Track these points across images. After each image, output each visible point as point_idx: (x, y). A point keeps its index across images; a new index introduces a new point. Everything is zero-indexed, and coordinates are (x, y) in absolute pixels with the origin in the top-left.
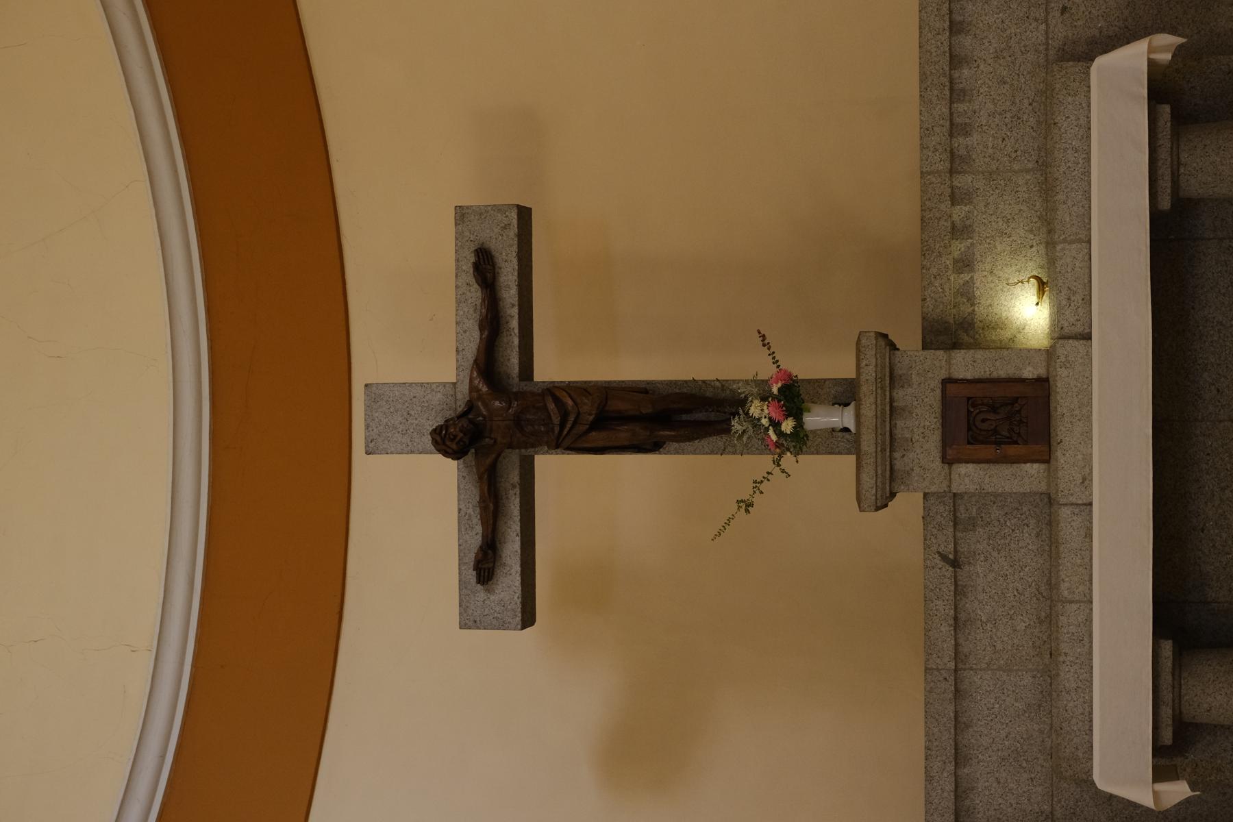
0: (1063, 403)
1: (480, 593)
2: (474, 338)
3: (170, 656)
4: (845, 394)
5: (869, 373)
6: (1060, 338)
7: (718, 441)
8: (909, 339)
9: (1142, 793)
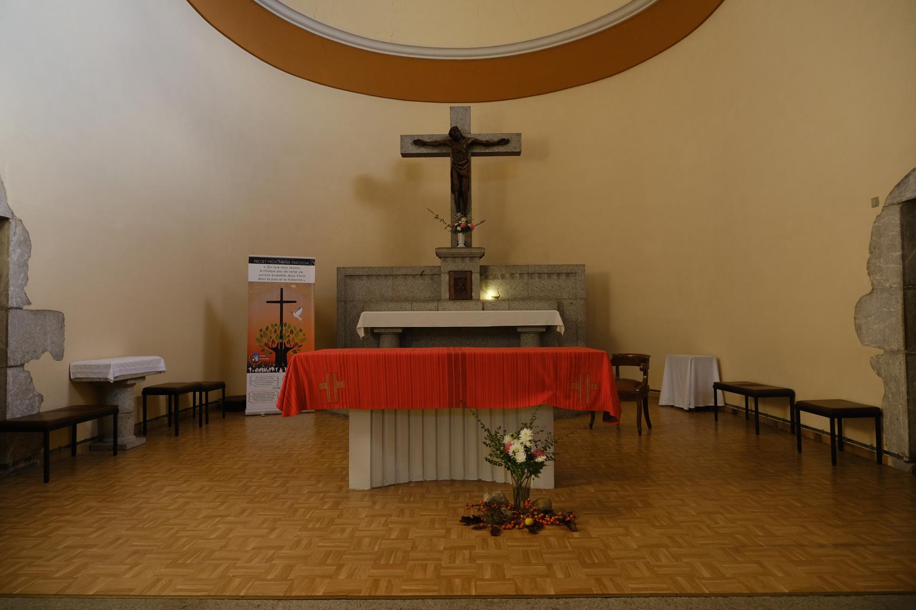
0: (465, 303)
2: (484, 139)
4: (468, 244)
5: (474, 251)
7: (454, 209)
8: (483, 262)
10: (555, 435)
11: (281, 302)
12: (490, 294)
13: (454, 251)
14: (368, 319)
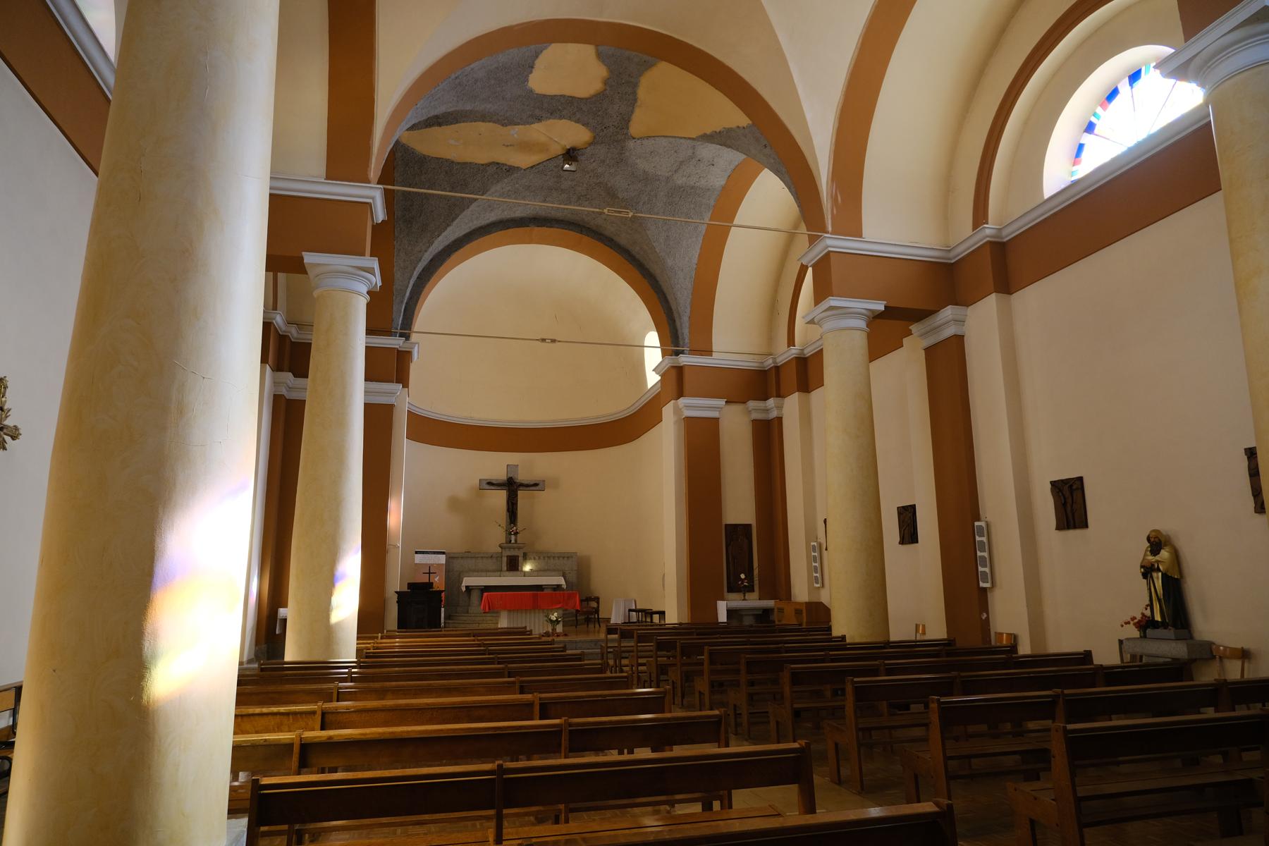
0: (515, 573)
1: (485, 482)
2: (526, 482)
3: (417, 409)
6: (540, 571)
7: (509, 521)
9: (464, 584)
11: (429, 573)
14: (468, 581)
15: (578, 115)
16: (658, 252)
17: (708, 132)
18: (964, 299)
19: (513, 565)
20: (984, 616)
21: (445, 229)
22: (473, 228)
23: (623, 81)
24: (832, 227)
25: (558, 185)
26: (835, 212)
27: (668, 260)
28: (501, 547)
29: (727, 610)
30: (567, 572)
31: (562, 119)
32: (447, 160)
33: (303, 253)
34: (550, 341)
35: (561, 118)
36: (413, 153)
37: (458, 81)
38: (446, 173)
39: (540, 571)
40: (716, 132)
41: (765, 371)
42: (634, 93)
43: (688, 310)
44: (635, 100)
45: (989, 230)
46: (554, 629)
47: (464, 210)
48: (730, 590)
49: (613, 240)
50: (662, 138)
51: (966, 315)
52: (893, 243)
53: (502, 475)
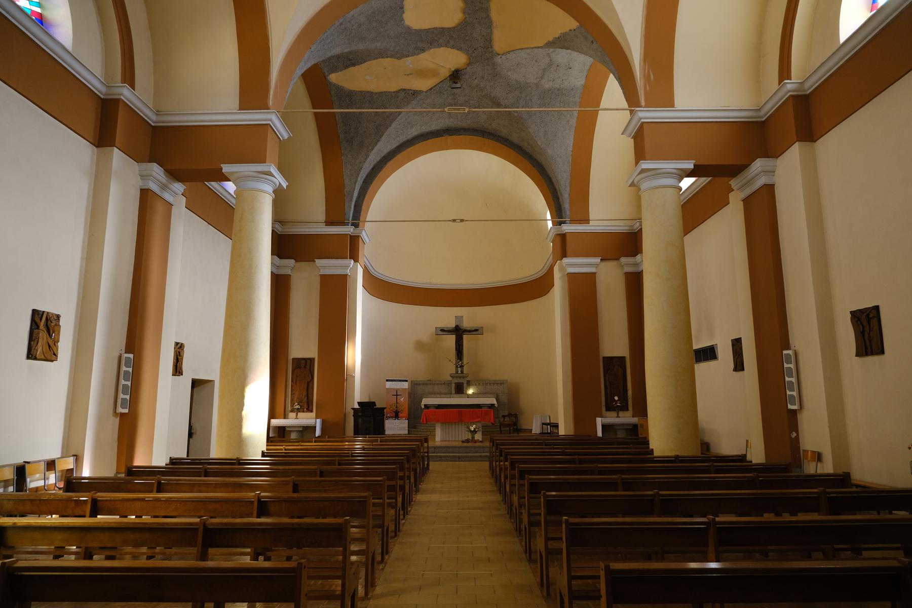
0: (461, 395)
2: (468, 329)
4: (462, 372)
5: (464, 375)
7: (457, 357)
8: (468, 379)
9: (423, 403)
10: (314, 44)
11: (397, 395)
12: (470, 391)
13: (457, 375)
15: (452, 43)
16: (540, 145)
17: (551, 40)
18: (772, 151)
19: (460, 390)
20: (794, 435)
21: (376, 144)
22: (401, 142)
23: (477, 9)
24: (645, 102)
25: (456, 101)
26: (648, 88)
27: (549, 151)
28: (453, 377)
29: (602, 425)
30: (500, 395)
31: (440, 47)
32: (368, 92)
33: (222, 165)
34: (459, 221)
35: (440, 46)
36: (342, 89)
37: (343, 27)
38: (370, 102)
39: (480, 393)
40: (556, 38)
41: (636, 232)
42: (488, 17)
43: (568, 189)
44: (491, 22)
45: (790, 86)
46: (473, 437)
47: (387, 128)
48: (609, 409)
49: (508, 140)
50: (520, 51)
51: (776, 166)
52: (703, 109)
53: (452, 324)
